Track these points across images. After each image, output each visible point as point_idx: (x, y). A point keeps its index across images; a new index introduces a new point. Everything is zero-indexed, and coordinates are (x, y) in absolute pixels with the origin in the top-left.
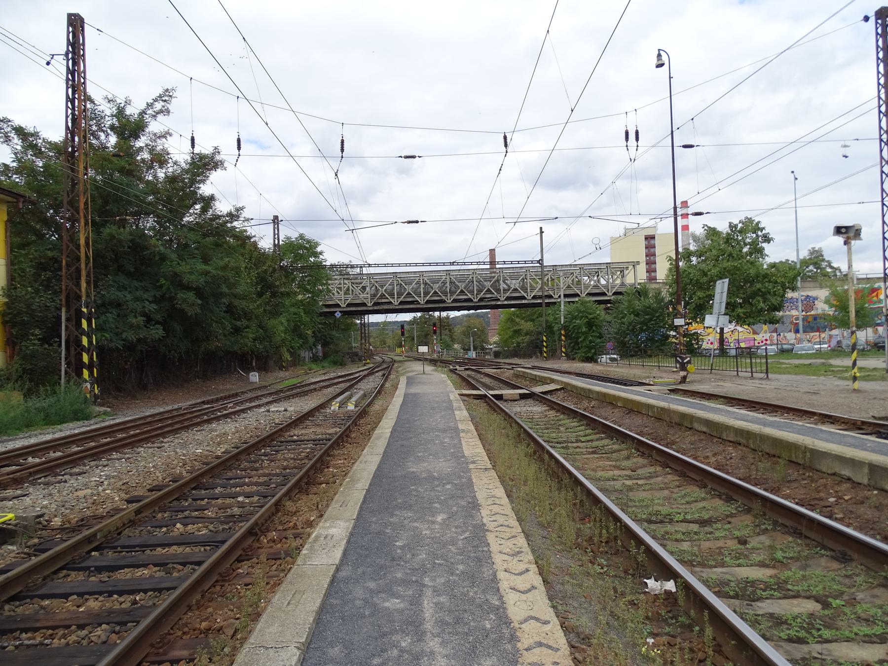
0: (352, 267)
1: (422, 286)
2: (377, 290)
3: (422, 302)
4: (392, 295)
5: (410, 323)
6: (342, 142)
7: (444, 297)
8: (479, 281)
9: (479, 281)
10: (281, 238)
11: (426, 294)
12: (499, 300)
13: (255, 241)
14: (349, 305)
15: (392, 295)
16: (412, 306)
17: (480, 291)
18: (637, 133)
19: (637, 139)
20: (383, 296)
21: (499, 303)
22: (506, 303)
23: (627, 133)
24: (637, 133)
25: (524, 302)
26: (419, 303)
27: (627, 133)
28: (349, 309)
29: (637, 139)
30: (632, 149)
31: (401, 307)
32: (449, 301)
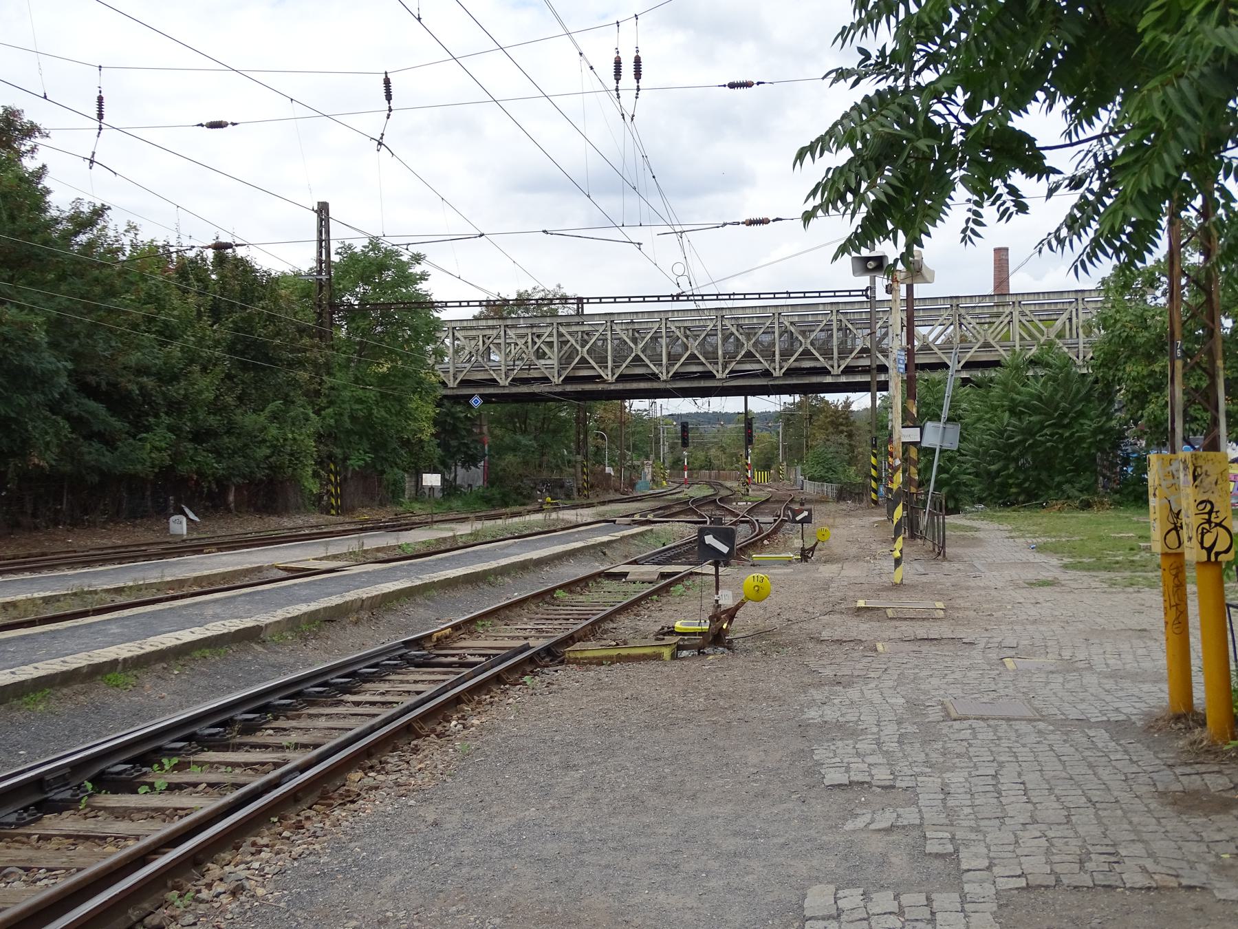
0: (564, 300)
1: (664, 341)
2: (739, 344)
3: (610, 379)
4: (827, 353)
5: (777, 416)
6: (100, 99)
7: (710, 367)
8: (673, 339)
9: (673, 339)
10: (334, 246)
11: (672, 358)
12: (828, 373)
13: (1031, 176)
14: (516, 381)
15: (827, 353)
16: (703, 384)
17: (786, 354)
18: (638, 61)
19: (638, 75)
20: (806, 354)
21: (829, 379)
22: (843, 379)
23: (618, 64)
24: (638, 61)
25: (600, 387)
26: (604, 381)
27: (618, 64)
28: (514, 390)
29: (638, 75)
30: (627, 97)
31: (620, 386)
32: (836, 371)
